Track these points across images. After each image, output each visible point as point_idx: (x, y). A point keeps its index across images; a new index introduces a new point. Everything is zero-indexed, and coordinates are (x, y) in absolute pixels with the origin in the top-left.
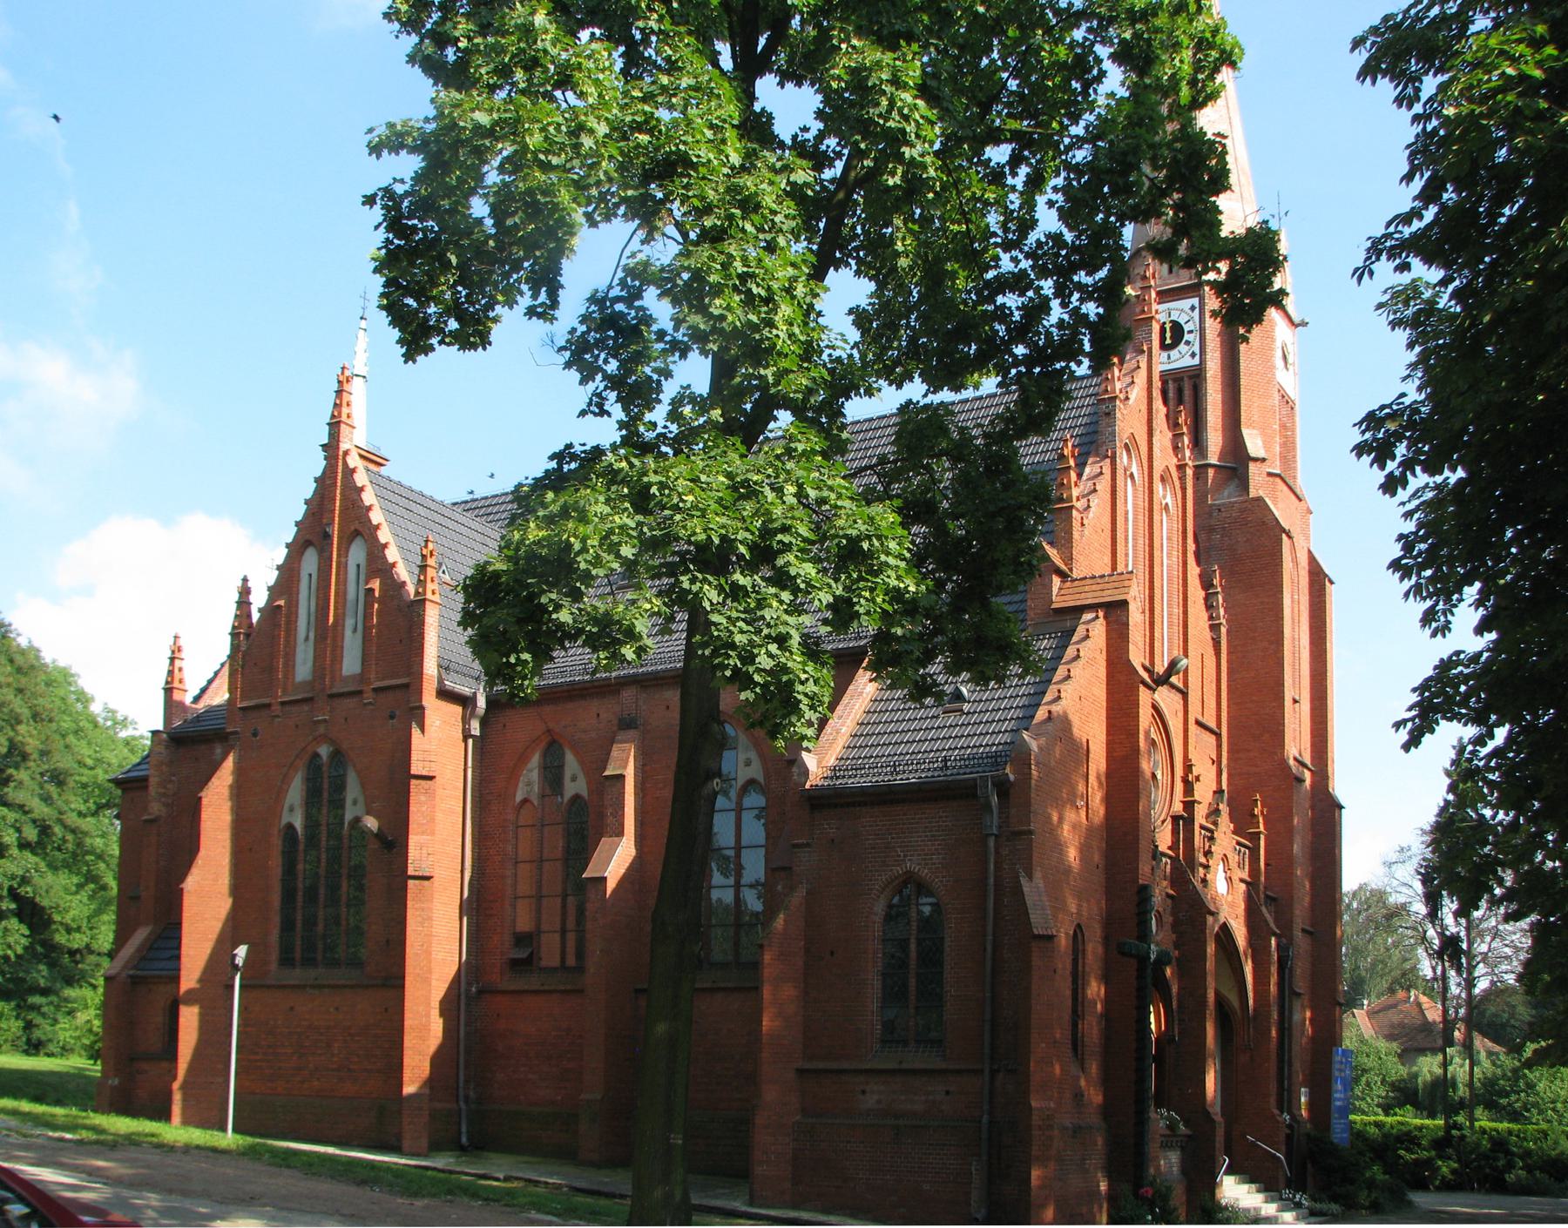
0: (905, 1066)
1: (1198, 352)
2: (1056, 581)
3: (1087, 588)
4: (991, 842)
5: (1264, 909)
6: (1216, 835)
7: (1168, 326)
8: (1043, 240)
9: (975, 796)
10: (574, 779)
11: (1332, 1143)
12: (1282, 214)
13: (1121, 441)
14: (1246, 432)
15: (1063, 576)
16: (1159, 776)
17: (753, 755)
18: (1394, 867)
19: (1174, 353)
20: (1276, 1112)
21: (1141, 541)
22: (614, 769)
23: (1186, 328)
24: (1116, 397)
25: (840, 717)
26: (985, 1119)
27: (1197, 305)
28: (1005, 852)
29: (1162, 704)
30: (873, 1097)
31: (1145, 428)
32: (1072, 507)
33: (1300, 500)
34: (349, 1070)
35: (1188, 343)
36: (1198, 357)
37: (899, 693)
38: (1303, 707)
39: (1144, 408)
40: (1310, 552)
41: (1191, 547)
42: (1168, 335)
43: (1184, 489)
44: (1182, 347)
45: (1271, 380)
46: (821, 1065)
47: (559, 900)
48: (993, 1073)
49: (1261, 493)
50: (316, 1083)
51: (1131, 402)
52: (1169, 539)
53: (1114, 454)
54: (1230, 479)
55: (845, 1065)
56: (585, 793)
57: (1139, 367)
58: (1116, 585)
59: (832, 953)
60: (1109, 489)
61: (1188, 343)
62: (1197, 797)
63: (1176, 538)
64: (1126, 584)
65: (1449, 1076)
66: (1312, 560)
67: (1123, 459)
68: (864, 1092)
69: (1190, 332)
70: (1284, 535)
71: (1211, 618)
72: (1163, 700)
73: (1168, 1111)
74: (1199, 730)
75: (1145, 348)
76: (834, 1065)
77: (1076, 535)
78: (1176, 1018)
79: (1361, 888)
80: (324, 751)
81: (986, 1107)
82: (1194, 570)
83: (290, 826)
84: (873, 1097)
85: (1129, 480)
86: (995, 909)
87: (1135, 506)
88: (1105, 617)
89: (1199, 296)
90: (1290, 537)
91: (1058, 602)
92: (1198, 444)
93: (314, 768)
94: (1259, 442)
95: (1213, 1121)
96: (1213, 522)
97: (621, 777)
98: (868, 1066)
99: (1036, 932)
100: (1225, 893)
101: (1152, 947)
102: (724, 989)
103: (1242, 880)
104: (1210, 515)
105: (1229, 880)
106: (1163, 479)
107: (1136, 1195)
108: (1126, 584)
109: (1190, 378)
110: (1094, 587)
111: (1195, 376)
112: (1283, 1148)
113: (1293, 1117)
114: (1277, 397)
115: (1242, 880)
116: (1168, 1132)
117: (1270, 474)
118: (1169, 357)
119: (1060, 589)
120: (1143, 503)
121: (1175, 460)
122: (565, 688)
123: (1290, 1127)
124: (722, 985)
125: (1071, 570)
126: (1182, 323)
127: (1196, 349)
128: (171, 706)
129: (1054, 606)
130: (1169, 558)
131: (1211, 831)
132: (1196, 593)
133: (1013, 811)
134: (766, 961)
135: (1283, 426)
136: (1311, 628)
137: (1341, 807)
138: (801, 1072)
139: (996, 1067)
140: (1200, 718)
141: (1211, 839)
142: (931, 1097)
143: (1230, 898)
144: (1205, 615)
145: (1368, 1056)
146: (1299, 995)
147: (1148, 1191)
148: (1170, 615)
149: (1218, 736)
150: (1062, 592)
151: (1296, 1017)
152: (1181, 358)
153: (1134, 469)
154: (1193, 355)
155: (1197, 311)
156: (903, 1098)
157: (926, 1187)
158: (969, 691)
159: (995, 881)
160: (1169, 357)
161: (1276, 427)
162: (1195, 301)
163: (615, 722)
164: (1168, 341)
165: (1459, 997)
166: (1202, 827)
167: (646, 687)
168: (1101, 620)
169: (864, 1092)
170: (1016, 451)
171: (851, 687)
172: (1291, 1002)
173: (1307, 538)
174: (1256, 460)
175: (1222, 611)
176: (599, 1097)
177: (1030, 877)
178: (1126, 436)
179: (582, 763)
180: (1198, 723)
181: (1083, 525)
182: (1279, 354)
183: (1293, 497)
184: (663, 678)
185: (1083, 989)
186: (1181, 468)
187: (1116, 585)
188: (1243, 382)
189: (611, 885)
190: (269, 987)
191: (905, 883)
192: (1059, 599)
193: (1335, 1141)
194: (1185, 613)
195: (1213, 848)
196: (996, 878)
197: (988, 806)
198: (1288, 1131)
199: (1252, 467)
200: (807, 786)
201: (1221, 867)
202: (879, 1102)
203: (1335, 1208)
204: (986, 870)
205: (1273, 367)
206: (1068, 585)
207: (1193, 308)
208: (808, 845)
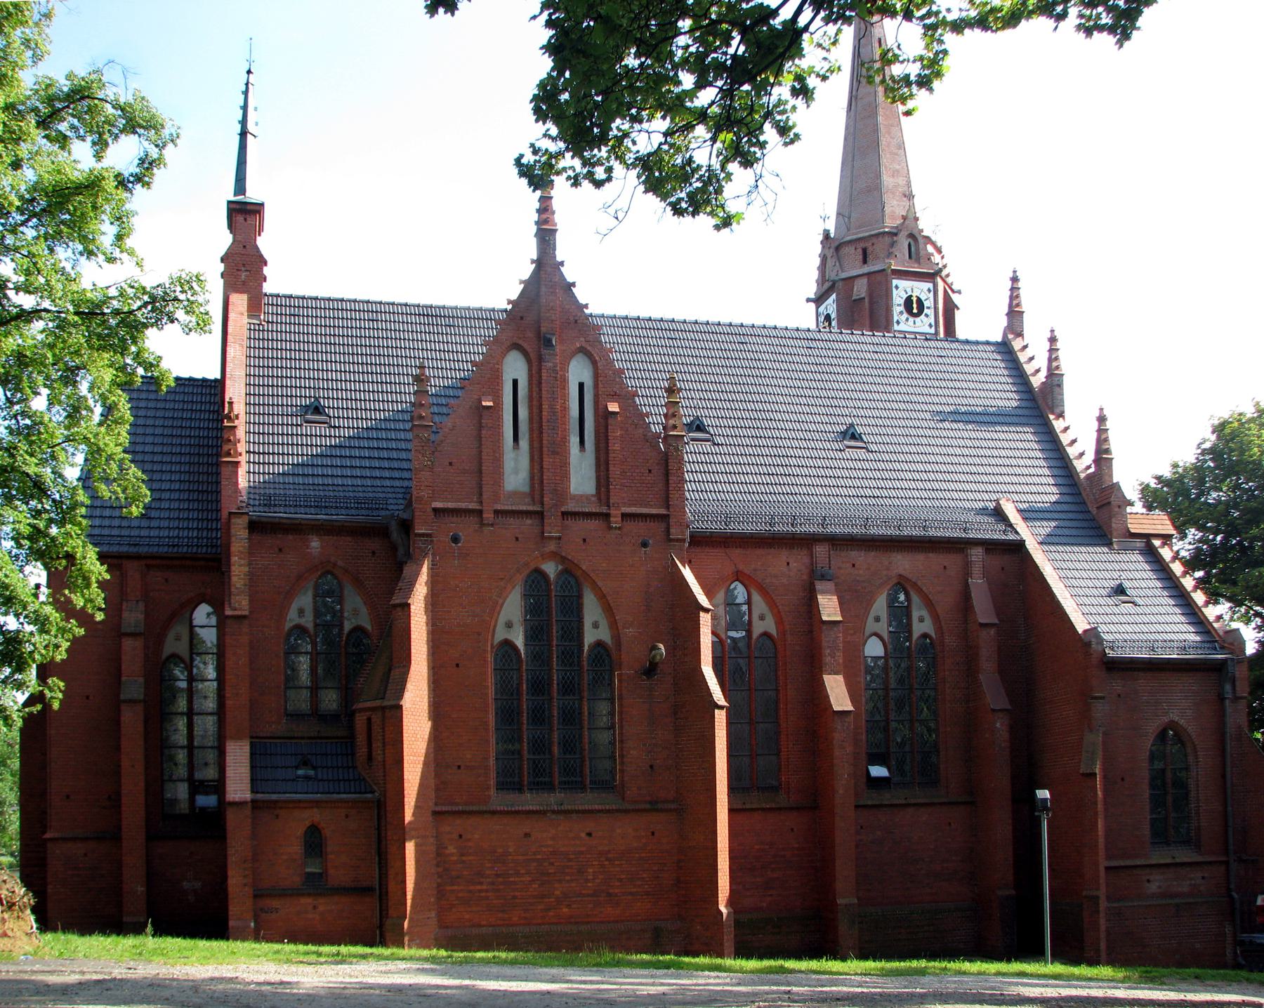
1: (933, 324)
10: (762, 618)
17: (924, 613)
30: (1156, 883)
34: (609, 895)
35: (927, 316)
50: (565, 910)
55: (1138, 862)
59: (1123, 779)
61: (927, 316)
68: (1148, 881)
69: (928, 308)
76: (1129, 862)
80: (551, 569)
83: (508, 644)
84: (1156, 883)
93: (536, 581)
102: (915, 805)
124: (913, 801)
157: (1198, 946)
164: (915, 311)
184: (839, 540)
190: (494, 813)
202: (1159, 887)
208: (1102, 698)
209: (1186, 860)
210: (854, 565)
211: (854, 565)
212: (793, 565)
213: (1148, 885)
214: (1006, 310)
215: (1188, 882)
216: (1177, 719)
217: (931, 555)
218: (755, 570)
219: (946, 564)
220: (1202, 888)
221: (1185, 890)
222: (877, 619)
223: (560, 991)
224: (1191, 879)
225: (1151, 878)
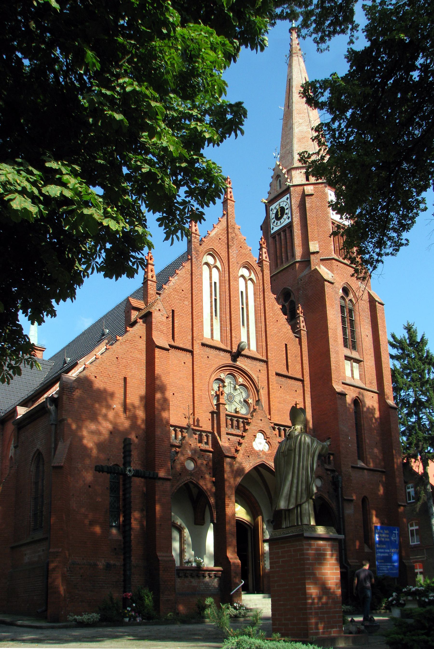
1: (290, 216)
19: (282, 220)
23: (286, 208)
27: (289, 197)
35: (286, 214)
36: (290, 218)
42: (279, 213)
44: (285, 216)
61: (286, 214)
70: (207, 508)
104: (298, 283)
127: (290, 215)
128: (188, 560)
134: (156, 499)
138: (12, 548)
149: (302, 381)
151: (19, 624)
155: (289, 199)
174: (314, 253)
185: (362, 408)
188: (308, 222)
199: (312, 257)
207: (287, 199)
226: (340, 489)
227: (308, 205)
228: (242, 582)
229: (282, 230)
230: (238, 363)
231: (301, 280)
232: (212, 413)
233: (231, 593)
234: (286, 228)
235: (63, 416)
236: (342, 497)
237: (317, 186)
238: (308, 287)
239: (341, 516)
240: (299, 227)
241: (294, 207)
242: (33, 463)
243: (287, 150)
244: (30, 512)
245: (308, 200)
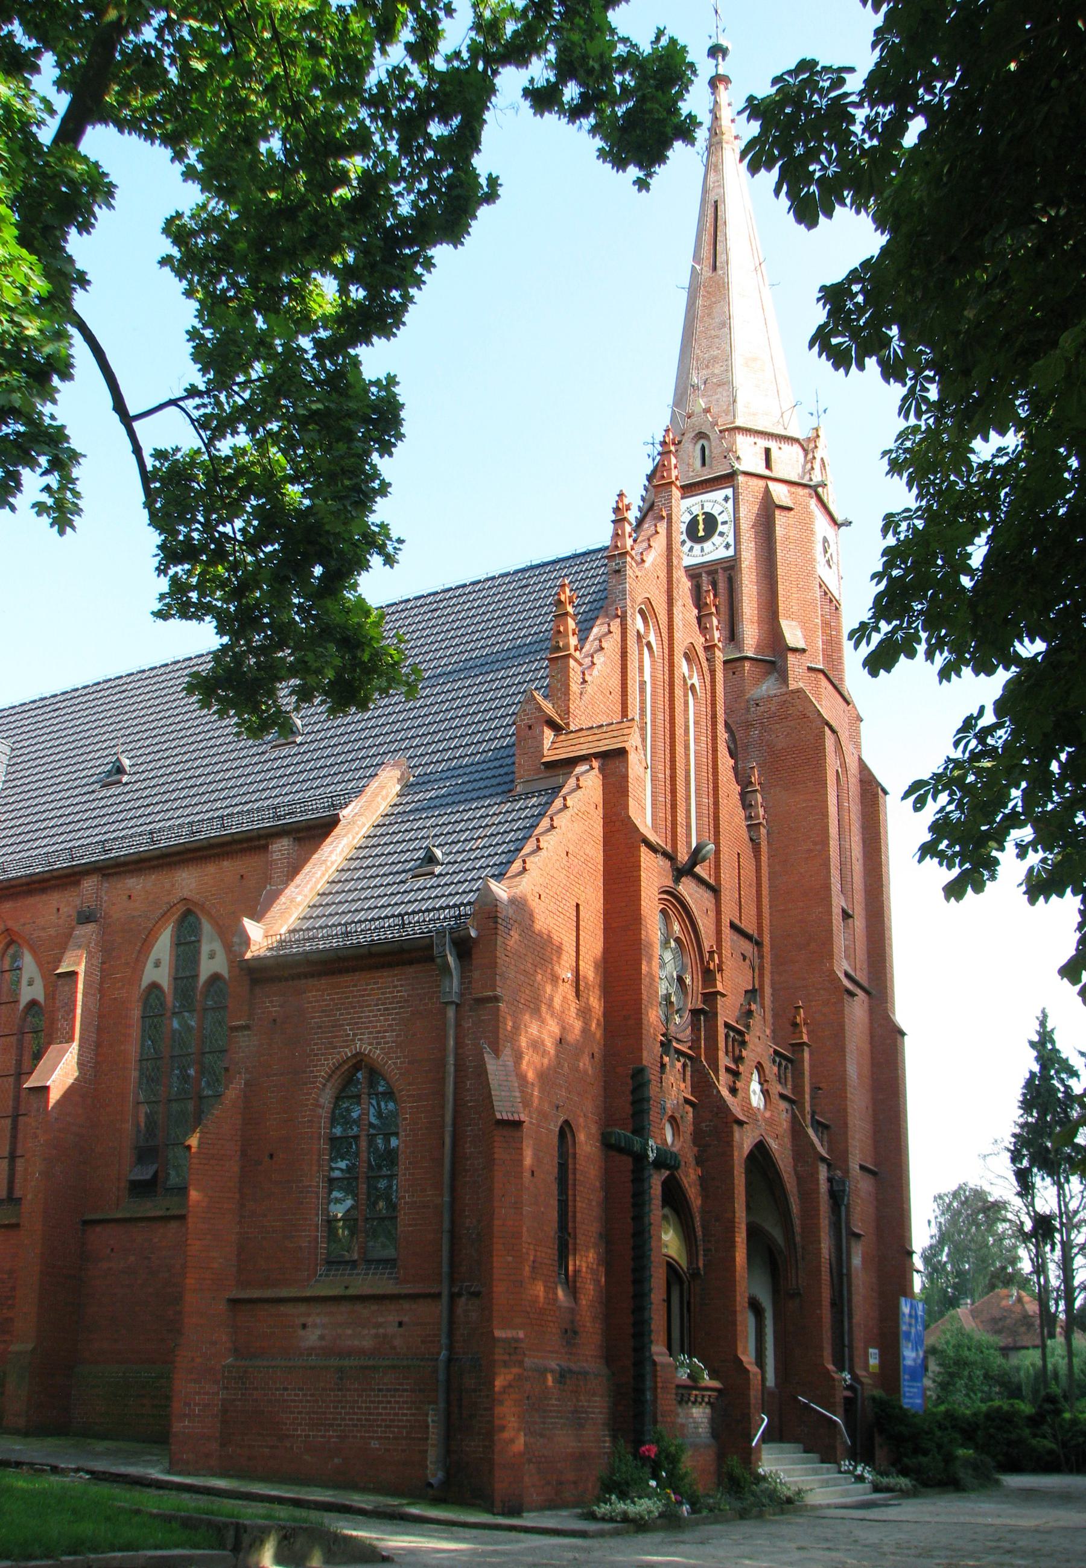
0: (351, 1292)
1: (732, 542)
2: (549, 735)
3: (582, 740)
4: (451, 1012)
5: (810, 1131)
6: (747, 1037)
7: (701, 518)
8: (386, 81)
9: (431, 959)
11: (901, 1408)
12: (821, 412)
13: (633, 600)
14: (784, 623)
15: (556, 728)
16: (688, 981)
17: (217, 946)
18: (988, 1159)
19: (708, 546)
20: (831, 1367)
21: (660, 716)
22: (69, 965)
23: (720, 519)
24: (627, 552)
25: (297, 886)
26: (444, 1354)
27: (731, 495)
28: (467, 1024)
29: (688, 899)
31: (665, 598)
32: (569, 655)
33: (848, 703)
35: (721, 534)
36: (732, 549)
37: (194, 699)
38: (857, 923)
39: (663, 575)
40: (860, 759)
41: (723, 735)
43: (713, 672)
44: (716, 539)
45: (811, 573)
46: (256, 1294)
47: (9, 1121)
48: (453, 1297)
49: (801, 685)
51: (646, 565)
52: (696, 723)
53: (625, 613)
54: (768, 673)
55: (284, 1293)
56: (41, 999)
57: (657, 532)
58: (615, 734)
59: (271, 1156)
60: (618, 650)
61: (721, 534)
62: (720, 987)
63: (706, 723)
64: (626, 731)
65: (1050, 1366)
66: (863, 767)
67: (637, 623)
71: (749, 818)
72: (690, 895)
73: (690, 1357)
74: (736, 937)
75: (664, 514)
76: (269, 1293)
77: (575, 687)
78: (701, 1248)
79: (960, 1188)
81: (444, 1341)
82: (726, 763)
85: (646, 649)
86: (455, 1094)
87: (653, 677)
88: (601, 770)
89: (733, 486)
90: (833, 731)
91: (549, 756)
92: (733, 635)
94: (799, 633)
95: (747, 1371)
96: (750, 717)
97: (74, 974)
98: (308, 1293)
99: (499, 1117)
100: (762, 1106)
101: (651, 1142)
103: (783, 1096)
104: (748, 710)
105: (765, 1093)
106: (687, 656)
107: (636, 1455)
108: (626, 731)
109: (725, 569)
110: (590, 738)
111: (730, 568)
112: (840, 1409)
113: (855, 1377)
114: (818, 593)
115: (783, 1096)
116: (689, 1383)
117: (810, 669)
118: (702, 550)
119: (553, 743)
120: (662, 676)
121: (703, 640)
122: (24, 880)
123: (850, 1388)
125: (568, 724)
126: (716, 514)
129: (545, 760)
130: (697, 742)
131: (741, 1033)
132: (730, 788)
133: (476, 975)
135: (826, 624)
136: (864, 841)
137: (902, 1034)
138: (234, 1302)
139: (456, 1290)
140: (737, 922)
141: (743, 1043)
142: (381, 1331)
143: (768, 1114)
144: (742, 814)
145: (969, 1349)
146: (858, 1236)
147: (650, 1450)
148: (698, 805)
149: (759, 944)
150: (556, 745)
152: (715, 550)
153: (652, 638)
154: (727, 546)
155: (731, 502)
156: (349, 1332)
157: (374, 1444)
158: (444, 854)
159: (456, 1060)
160: (702, 550)
161: (819, 621)
162: (729, 492)
163: (75, 915)
164: (701, 533)
165: (1058, 1288)
166: (727, 1025)
167: (109, 875)
168: (596, 771)
169: (304, 1326)
170: (356, 363)
171: (315, 856)
172: (848, 1243)
173: (858, 746)
174: (795, 650)
175: (761, 811)
176: (30, 1346)
177: (497, 1052)
178: (640, 600)
179: (40, 965)
180: (733, 926)
181: (584, 681)
182: (819, 548)
183: (840, 699)
184: (125, 864)
186: (709, 648)
187: (615, 734)
188: (779, 572)
189: (54, 1096)
191: (357, 1067)
192: (551, 752)
193: (905, 1406)
194: (716, 803)
195: (744, 1053)
196: (457, 1055)
197: (446, 969)
198: (848, 1393)
199: (791, 658)
200: (248, 955)
201: (755, 1076)
202: (322, 1337)
203: (904, 1482)
204: (443, 1048)
205: (812, 560)
206: (562, 737)
207: (726, 499)
208: (247, 1027)
209: (367, 1291)
210: (130, 897)
211: (130, 897)
212: (64, 910)
213: (301, 1332)
214: (141, 497)
215: (373, 1331)
216: (366, 1048)
217: (225, 863)
218: (24, 925)
219: (243, 872)
220: (397, 1342)
221: (367, 1344)
222: (157, 964)
223: (432, 1540)
224: (379, 1325)
225: (309, 1321)
226: (843, 1208)
227: (779, 531)
228: (763, 1420)
229: (706, 569)
230: (681, 888)
231: (757, 705)
232: (695, 1013)
233: (754, 1444)
234: (719, 567)
235: (498, 989)
236: (848, 1227)
237: (793, 489)
238: (778, 726)
239: (845, 1271)
240: (754, 577)
241: (745, 525)
242: (329, 1085)
243: (713, 375)
244: (317, 1215)
245: (780, 518)
